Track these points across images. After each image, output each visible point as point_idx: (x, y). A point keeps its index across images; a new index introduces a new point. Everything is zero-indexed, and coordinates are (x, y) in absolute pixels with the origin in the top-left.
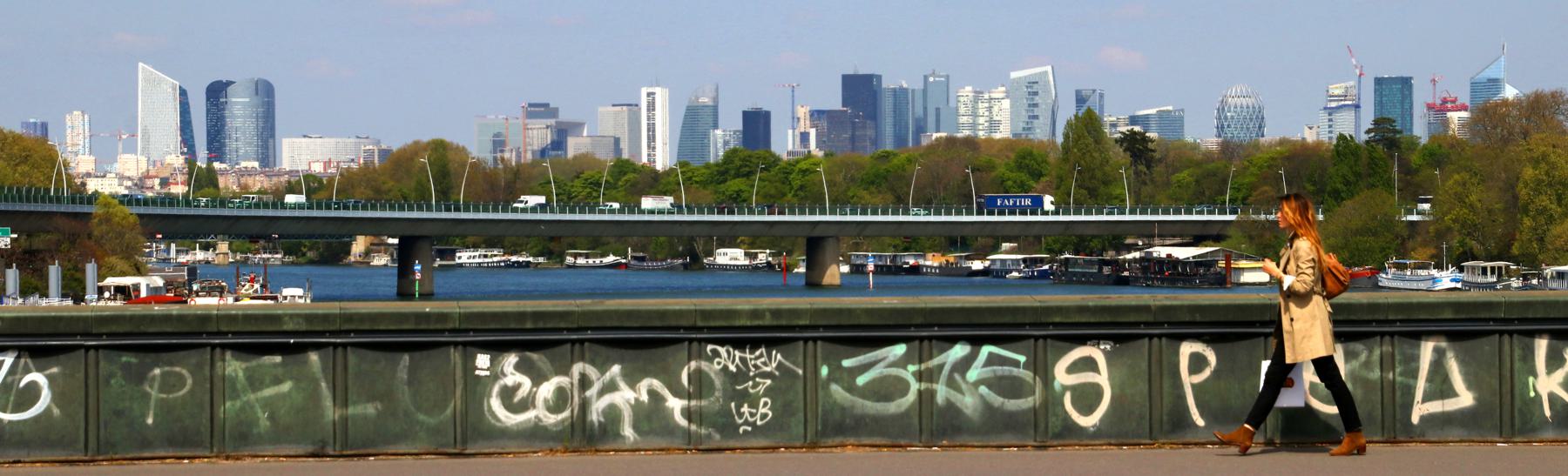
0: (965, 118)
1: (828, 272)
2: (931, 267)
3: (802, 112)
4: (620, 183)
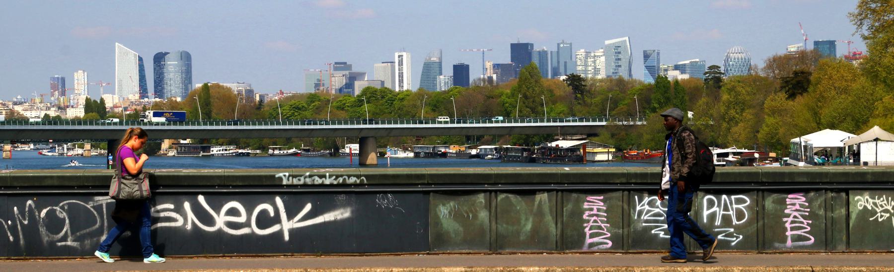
0: (581, 67)
1: (370, 157)
2: (452, 153)
3: (489, 65)
4: (310, 107)
